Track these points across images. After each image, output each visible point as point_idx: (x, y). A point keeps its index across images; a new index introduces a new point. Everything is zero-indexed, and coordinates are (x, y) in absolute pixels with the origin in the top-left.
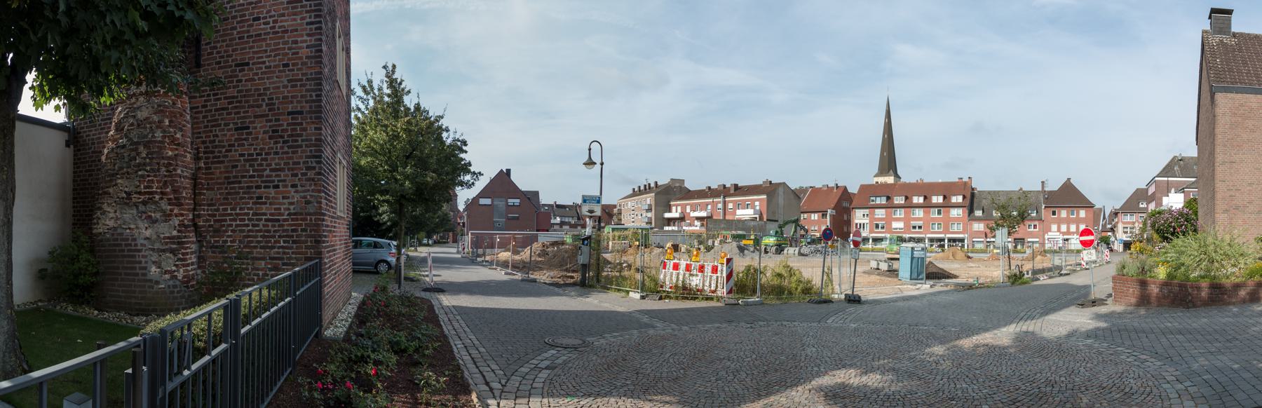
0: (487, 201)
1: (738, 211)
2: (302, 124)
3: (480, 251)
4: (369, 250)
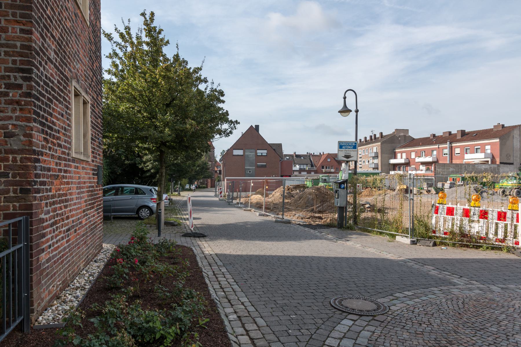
0: (240, 152)
1: (466, 155)
3: (235, 194)
4: (130, 197)
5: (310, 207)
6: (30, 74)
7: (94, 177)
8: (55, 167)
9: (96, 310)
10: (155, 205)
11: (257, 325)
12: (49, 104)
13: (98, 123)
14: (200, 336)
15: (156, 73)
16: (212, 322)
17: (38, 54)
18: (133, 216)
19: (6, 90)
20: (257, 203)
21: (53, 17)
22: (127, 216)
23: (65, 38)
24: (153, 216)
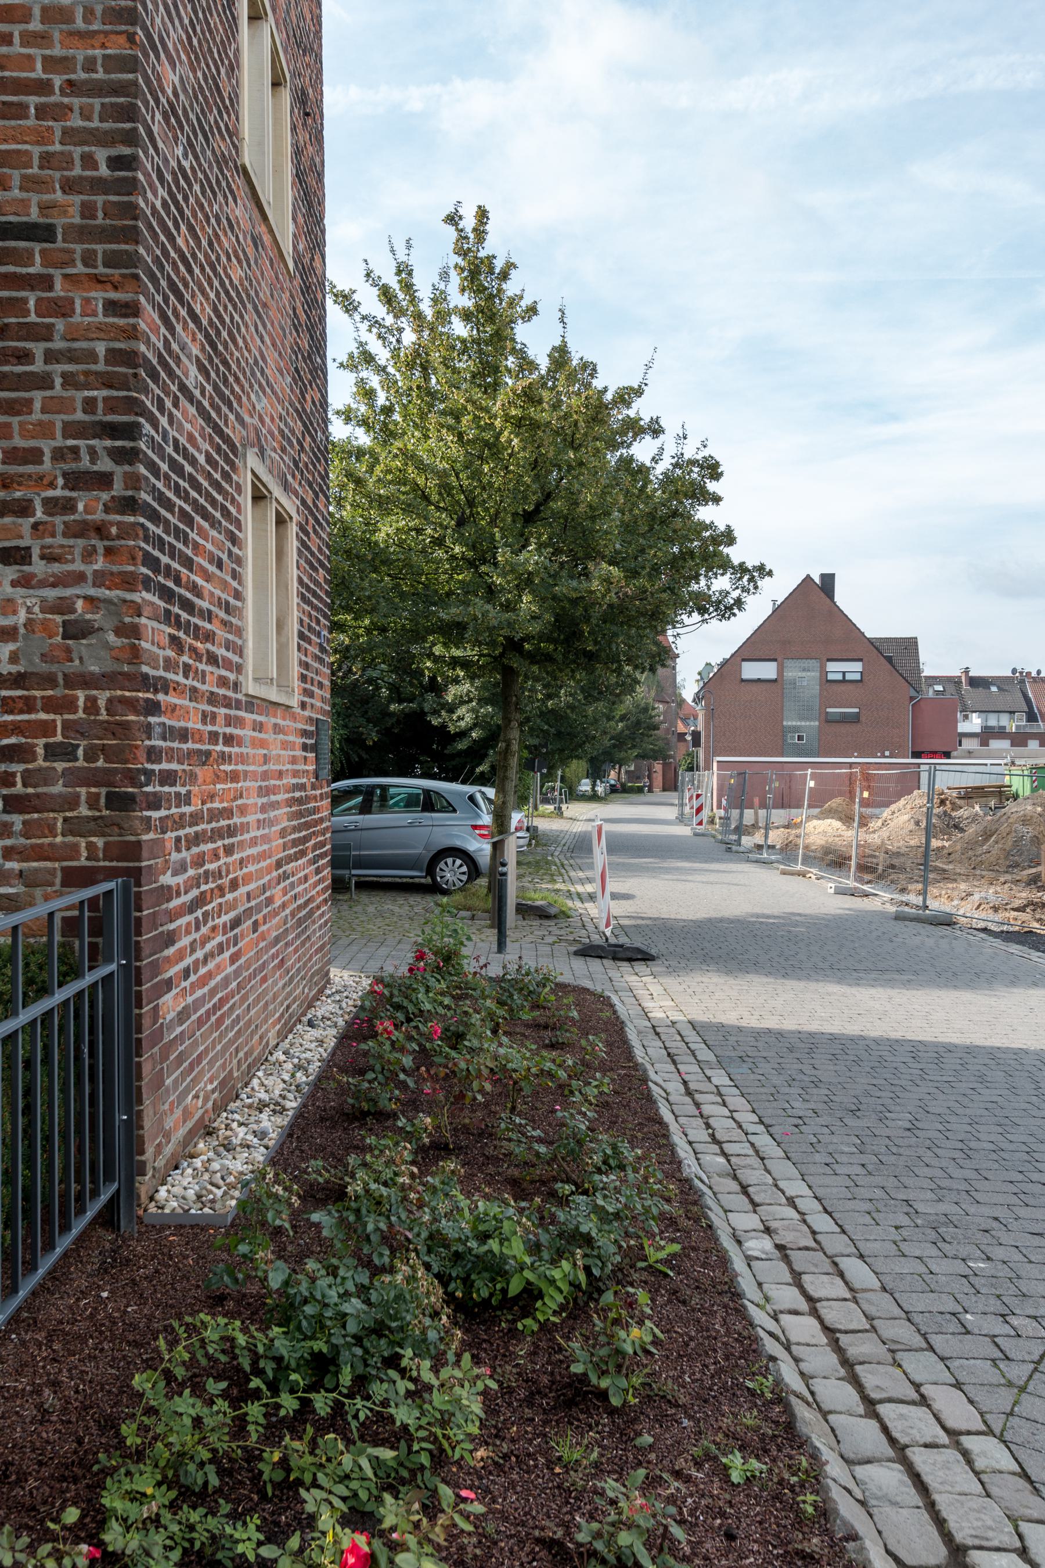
0: (767, 670)
2: (45, 282)
3: (749, 815)
4: (406, 818)
5: (1024, 869)
6: (134, 439)
7: (305, 758)
8: (199, 726)
9: (321, 1180)
10: (487, 848)
11: (846, 1283)
12: (184, 531)
13: (316, 583)
14: (653, 1300)
15: (494, 409)
16: (688, 1256)
17: (154, 376)
18: (417, 880)
19: (67, 493)
20: (827, 850)
21: (194, 256)
22: (398, 880)
23: (228, 320)
24: (478, 881)
